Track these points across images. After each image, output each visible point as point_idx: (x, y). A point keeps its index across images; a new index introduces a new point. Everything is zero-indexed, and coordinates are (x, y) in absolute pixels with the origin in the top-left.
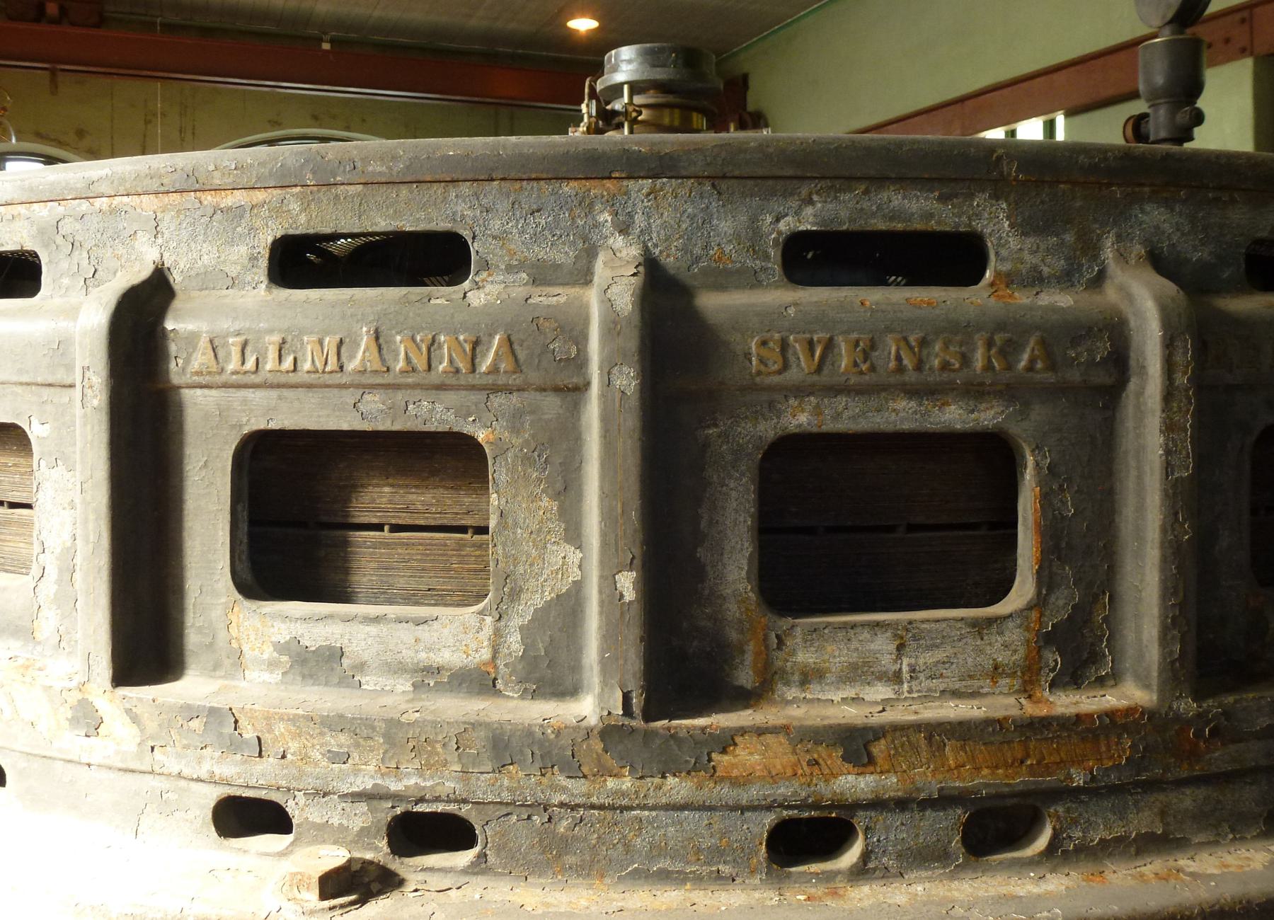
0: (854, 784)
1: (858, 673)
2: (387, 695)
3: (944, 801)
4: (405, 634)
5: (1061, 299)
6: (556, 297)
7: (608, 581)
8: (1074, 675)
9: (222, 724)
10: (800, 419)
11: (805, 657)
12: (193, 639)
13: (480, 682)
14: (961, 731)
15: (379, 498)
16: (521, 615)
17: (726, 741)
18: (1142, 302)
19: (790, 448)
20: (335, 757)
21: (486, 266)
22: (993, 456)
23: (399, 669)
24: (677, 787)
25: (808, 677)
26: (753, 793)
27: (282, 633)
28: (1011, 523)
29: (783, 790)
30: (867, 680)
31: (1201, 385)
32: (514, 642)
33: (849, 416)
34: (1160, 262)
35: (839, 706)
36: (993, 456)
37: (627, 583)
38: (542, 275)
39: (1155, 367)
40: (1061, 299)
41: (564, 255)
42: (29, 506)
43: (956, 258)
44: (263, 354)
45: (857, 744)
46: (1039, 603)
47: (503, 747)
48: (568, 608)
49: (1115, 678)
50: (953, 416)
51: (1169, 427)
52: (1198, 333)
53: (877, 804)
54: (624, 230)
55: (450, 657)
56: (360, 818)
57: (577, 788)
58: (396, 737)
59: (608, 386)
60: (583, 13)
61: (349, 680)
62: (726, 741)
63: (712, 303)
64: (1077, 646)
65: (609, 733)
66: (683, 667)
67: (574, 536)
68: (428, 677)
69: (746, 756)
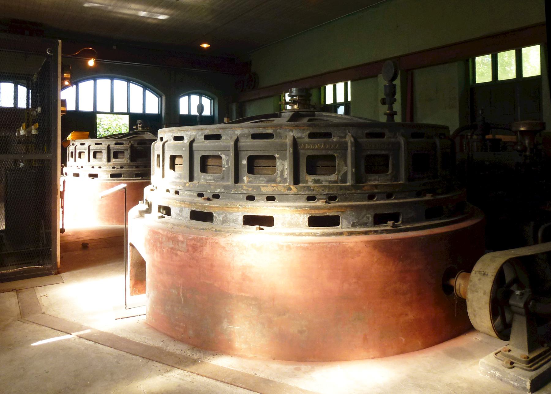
0: (376, 191)
1: (375, 180)
2: (324, 184)
3: (384, 193)
4: (327, 177)
5: (393, 140)
6: (343, 140)
7: (352, 170)
8: (395, 181)
9: (308, 188)
10: (369, 153)
11: (369, 178)
12: (301, 179)
13: (335, 182)
14: (386, 185)
15: (320, 163)
16: (340, 175)
17: (363, 186)
18: (402, 140)
19: (368, 156)
20: (323, 190)
21: (334, 136)
22: (386, 157)
23: (326, 181)
24: (359, 191)
25: (370, 180)
26: (366, 192)
27: (313, 178)
28: (388, 165)
29: (369, 191)
30: (375, 181)
31: (356, 151)
32: (340, 178)
33: (373, 153)
34: (403, 135)
35: (373, 183)
36: (386, 157)
37: (354, 170)
38: (341, 137)
39: (403, 146)
40: (393, 140)
41: (343, 135)
42: (163, 176)
43: (381, 135)
44: (251, 146)
45: (376, 186)
46: (392, 173)
47: (341, 188)
48: (346, 174)
49: (399, 181)
50: (383, 152)
51: (405, 153)
52: (407, 143)
53: (378, 193)
54: (349, 132)
55: (332, 179)
56: (325, 197)
57: (348, 192)
58: (330, 188)
59: (290, 151)
60: (205, 43)
61: (321, 183)
62: (363, 186)
63: (359, 140)
64: (396, 177)
65: (352, 186)
66: (359, 180)
67: (346, 166)
68: (330, 182)
69: (366, 188)
